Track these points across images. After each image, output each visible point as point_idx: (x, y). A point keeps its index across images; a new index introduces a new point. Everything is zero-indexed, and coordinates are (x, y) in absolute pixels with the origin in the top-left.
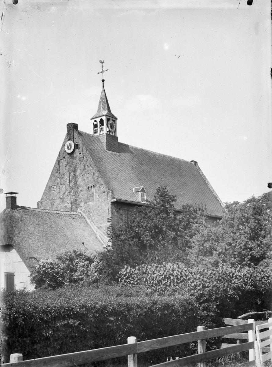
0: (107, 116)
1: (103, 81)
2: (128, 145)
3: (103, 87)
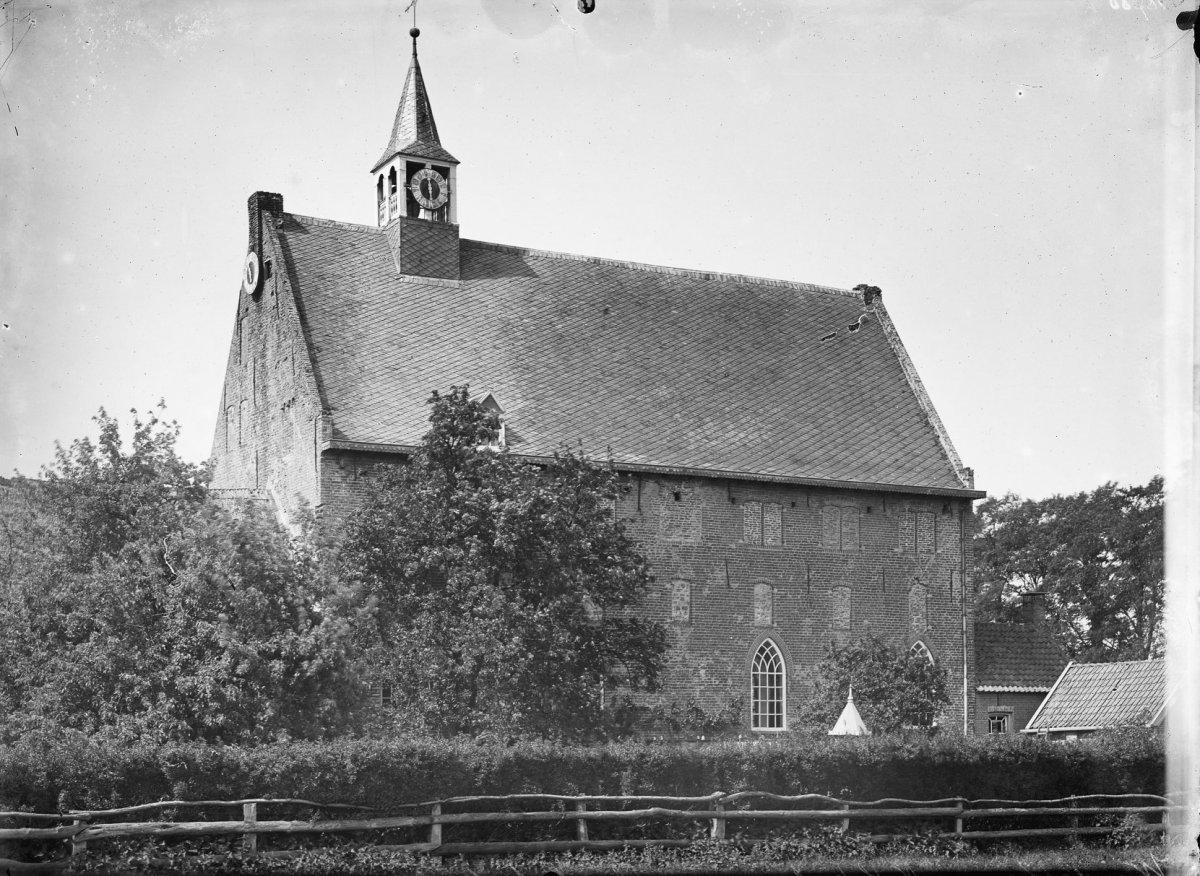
0: (409, 155)
1: (415, 34)
2: (525, 251)
3: (415, 54)
